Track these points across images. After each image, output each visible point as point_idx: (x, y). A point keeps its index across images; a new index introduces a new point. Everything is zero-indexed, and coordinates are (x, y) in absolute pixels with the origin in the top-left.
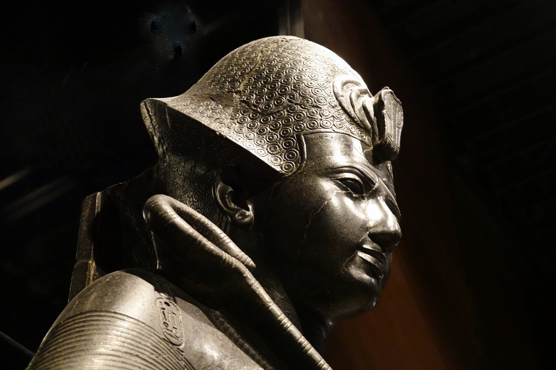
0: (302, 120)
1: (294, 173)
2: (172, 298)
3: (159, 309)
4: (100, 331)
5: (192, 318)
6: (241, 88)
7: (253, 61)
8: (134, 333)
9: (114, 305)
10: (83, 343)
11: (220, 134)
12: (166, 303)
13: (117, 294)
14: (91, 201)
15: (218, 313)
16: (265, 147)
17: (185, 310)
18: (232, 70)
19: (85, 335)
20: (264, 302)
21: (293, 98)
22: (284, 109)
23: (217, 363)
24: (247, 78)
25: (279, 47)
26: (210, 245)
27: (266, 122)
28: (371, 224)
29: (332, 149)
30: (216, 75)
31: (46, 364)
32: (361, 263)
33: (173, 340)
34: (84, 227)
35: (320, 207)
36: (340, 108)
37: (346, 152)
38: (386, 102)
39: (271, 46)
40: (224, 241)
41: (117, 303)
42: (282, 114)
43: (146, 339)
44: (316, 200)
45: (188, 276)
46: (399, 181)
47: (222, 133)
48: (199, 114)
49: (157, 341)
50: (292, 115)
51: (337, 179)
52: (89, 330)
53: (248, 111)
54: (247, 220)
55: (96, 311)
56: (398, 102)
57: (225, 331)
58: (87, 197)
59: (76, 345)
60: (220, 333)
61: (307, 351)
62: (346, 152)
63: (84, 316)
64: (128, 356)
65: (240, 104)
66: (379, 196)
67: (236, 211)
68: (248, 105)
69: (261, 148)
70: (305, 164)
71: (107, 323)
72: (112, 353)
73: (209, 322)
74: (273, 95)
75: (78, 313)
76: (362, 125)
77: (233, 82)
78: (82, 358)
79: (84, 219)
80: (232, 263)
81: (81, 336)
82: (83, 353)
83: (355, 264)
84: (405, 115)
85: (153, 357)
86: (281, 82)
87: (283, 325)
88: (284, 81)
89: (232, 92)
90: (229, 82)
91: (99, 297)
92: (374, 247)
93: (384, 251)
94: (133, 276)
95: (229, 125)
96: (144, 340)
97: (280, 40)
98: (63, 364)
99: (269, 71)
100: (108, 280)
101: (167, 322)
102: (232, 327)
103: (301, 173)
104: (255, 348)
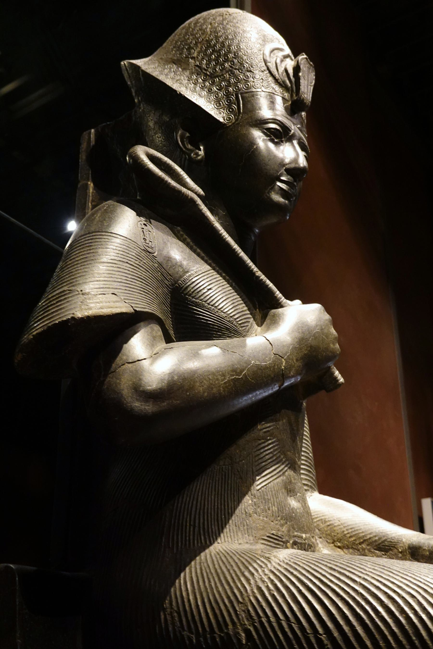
0: (239, 82)
1: (233, 123)
2: (148, 220)
3: (140, 229)
4: (102, 246)
5: (162, 234)
6: (195, 55)
7: (204, 32)
8: (125, 247)
9: (110, 227)
10: (91, 255)
11: (180, 93)
12: (144, 224)
13: (112, 219)
15: (179, 228)
16: (213, 103)
17: (157, 228)
18: (188, 39)
19: (93, 249)
20: (210, 221)
21: (234, 64)
22: (226, 73)
23: (179, 264)
25: (223, 20)
26: (173, 183)
27: (213, 83)
28: (287, 161)
29: (260, 105)
30: (176, 42)
31: (70, 269)
32: (280, 190)
33: (150, 250)
34: (83, 157)
35: (251, 150)
36: (268, 72)
37: (271, 106)
38: (301, 67)
39: (218, 18)
40: (183, 178)
41: (112, 226)
42: (225, 77)
43: (132, 250)
45: (159, 205)
46: (311, 127)
47: (182, 93)
48: (164, 76)
49: (139, 252)
50: (232, 77)
51: (264, 129)
52: (95, 245)
54: (199, 158)
55: (99, 232)
56: (311, 65)
57: (184, 241)
58: (85, 133)
59: (88, 256)
60: (180, 243)
61: (238, 254)
62: (271, 106)
63: (91, 235)
64: (121, 263)
65: (195, 68)
66: (294, 140)
67: (192, 151)
69: (209, 104)
70: (241, 117)
71: (107, 240)
72: (111, 261)
73: (173, 235)
74: (218, 61)
75: (87, 232)
76: (283, 85)
77: (189, 49)
78: (93, 265)
79: (83, 150)
80: (188, 195)
81: (90, 250)
82: (93, 262)
83: (274, 191)
84: (316, 75)
85: (137, 262)
86: (225, 51)
87: (223, 237)
88: (227, 50)
89: (188, 58)
90: (186, 49)
91: (100, 221)
92: (288, 179)
93: (295, 181)
94: (122, 205)
95: (187, 85)
96: (131, 251)
97: (225, 14)
98: (81, 269)
99: (216, 41)
100: (105, 208)
101: (145, 238)
102: (189, 238)
103: (238, 124)
104: (204, 252)
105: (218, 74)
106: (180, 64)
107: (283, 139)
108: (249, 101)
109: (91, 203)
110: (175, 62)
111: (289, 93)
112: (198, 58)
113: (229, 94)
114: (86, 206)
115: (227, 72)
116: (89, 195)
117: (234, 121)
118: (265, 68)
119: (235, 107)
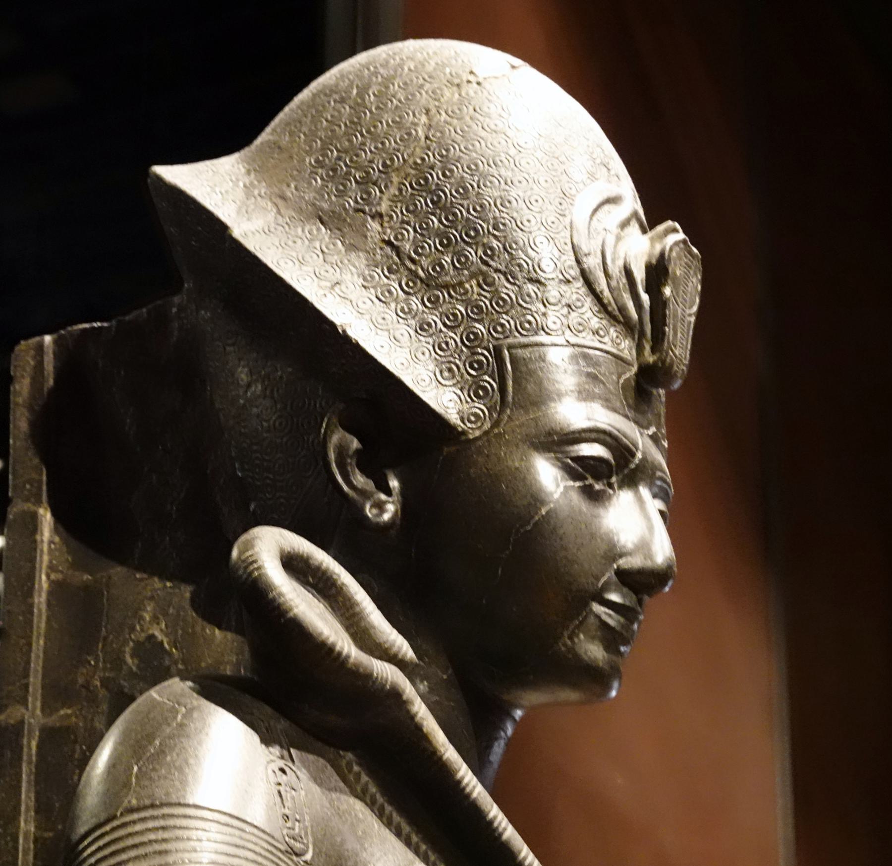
1: (486, 433)
7: (408, 137)
11: (344, 331)
14: (34, 358)
15: (350, 756)
24: (395, 180)
34: (20, 422)
35: (533, 517)
44: (525, 503)
53: (397, 271)
68: (398, 256)
75: (147, 802)
76: (622, 319)
79: (20, 400)
87: (459, 782)
90: (357, 182)
105: (448, 278)
106: (339, 229)
107: (614, 479)
108: (531, 373)
109: (48, 576)
110: (325, 218)
111: (633, 339)
112: (391, 217)
113: (476, 343)
114: (33, 585)
115: (473, 276)
116: (42, 551)
117: (487, 426)
118: (575, 272)
119: (491, 386)
